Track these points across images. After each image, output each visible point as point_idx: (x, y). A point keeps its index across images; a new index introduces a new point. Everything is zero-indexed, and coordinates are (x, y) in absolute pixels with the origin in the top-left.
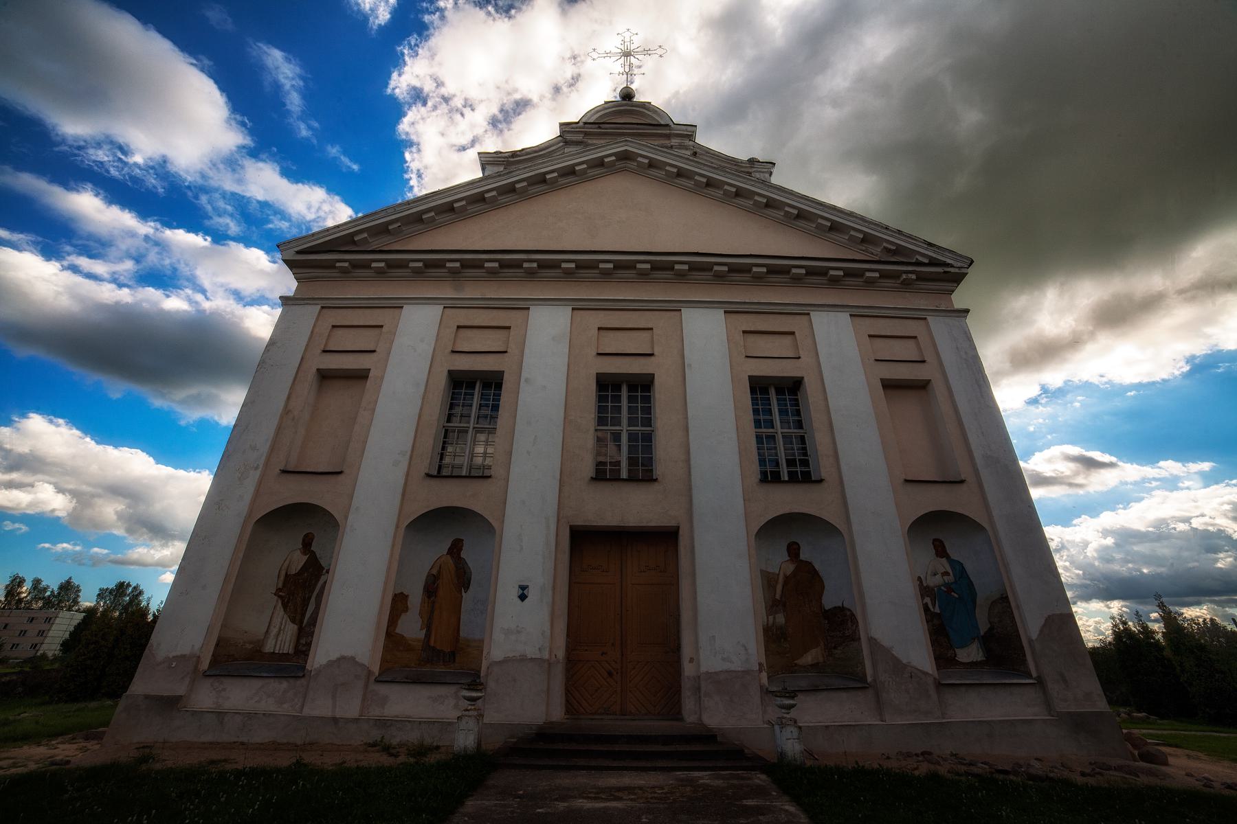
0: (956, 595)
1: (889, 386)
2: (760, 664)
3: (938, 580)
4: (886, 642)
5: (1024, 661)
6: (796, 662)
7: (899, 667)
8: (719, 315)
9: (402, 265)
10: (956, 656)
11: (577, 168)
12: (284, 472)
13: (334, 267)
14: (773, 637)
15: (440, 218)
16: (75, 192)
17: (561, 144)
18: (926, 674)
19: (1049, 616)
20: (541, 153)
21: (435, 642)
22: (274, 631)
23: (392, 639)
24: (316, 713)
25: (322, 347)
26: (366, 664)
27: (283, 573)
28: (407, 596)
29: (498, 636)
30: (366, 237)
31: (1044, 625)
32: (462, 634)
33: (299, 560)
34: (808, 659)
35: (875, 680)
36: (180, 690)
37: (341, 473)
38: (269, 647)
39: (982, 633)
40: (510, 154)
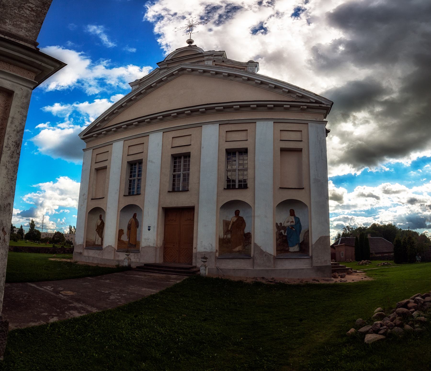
0: (294, 230)
1: (283, 150)
2: (217, 250)
3: (289, 224)
4: (259, 245)
5: (308, 251)
6: (233, 250)
7: (262, 252)
8: (217, 126)
9: (110, 130)
10: (289, 249)
11: (174, 73)
12: (92, 199)
13: (93, 137)
14: (222, 242)
15: (120, 111)
16: (59, 110)
17: (158, 70)
18: (271, 255)
19: (321, 237)
20: (151, 76)
21: (131, 242)
22: (97, 239)
23: (120, 240)
24: (105, 258)
25: (95, 162)
26: (114, 247)
27: (97, 225)
28: (123, 230)
29: (143, 240)
30: (100, 124)
31: (318, 240)
32: (137, 240)
33: (100, 222)
34: (237, 249)
35: (254, 256)
36: (82, 251)
37: (104, 198)
38: (96, 243)
39: (300, 242)
40: (139, 80)
